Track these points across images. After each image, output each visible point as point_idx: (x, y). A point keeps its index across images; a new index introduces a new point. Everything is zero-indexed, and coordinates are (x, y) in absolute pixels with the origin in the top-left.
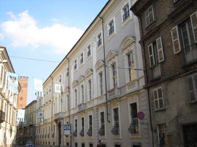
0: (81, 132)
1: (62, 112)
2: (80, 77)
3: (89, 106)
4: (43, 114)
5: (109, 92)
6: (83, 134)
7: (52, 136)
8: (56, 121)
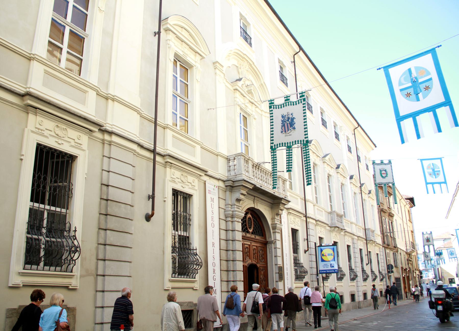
4: (299, 123)
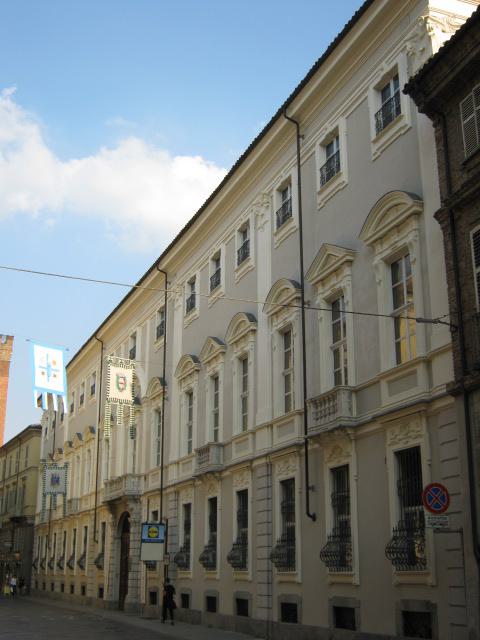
0: (99, 558)
1: (136, 472)
2: (208, 341)
3: (236, 455)
5: (316, 402)
6: (211, 560)
7: (96, 562)
8: (112, 505)
